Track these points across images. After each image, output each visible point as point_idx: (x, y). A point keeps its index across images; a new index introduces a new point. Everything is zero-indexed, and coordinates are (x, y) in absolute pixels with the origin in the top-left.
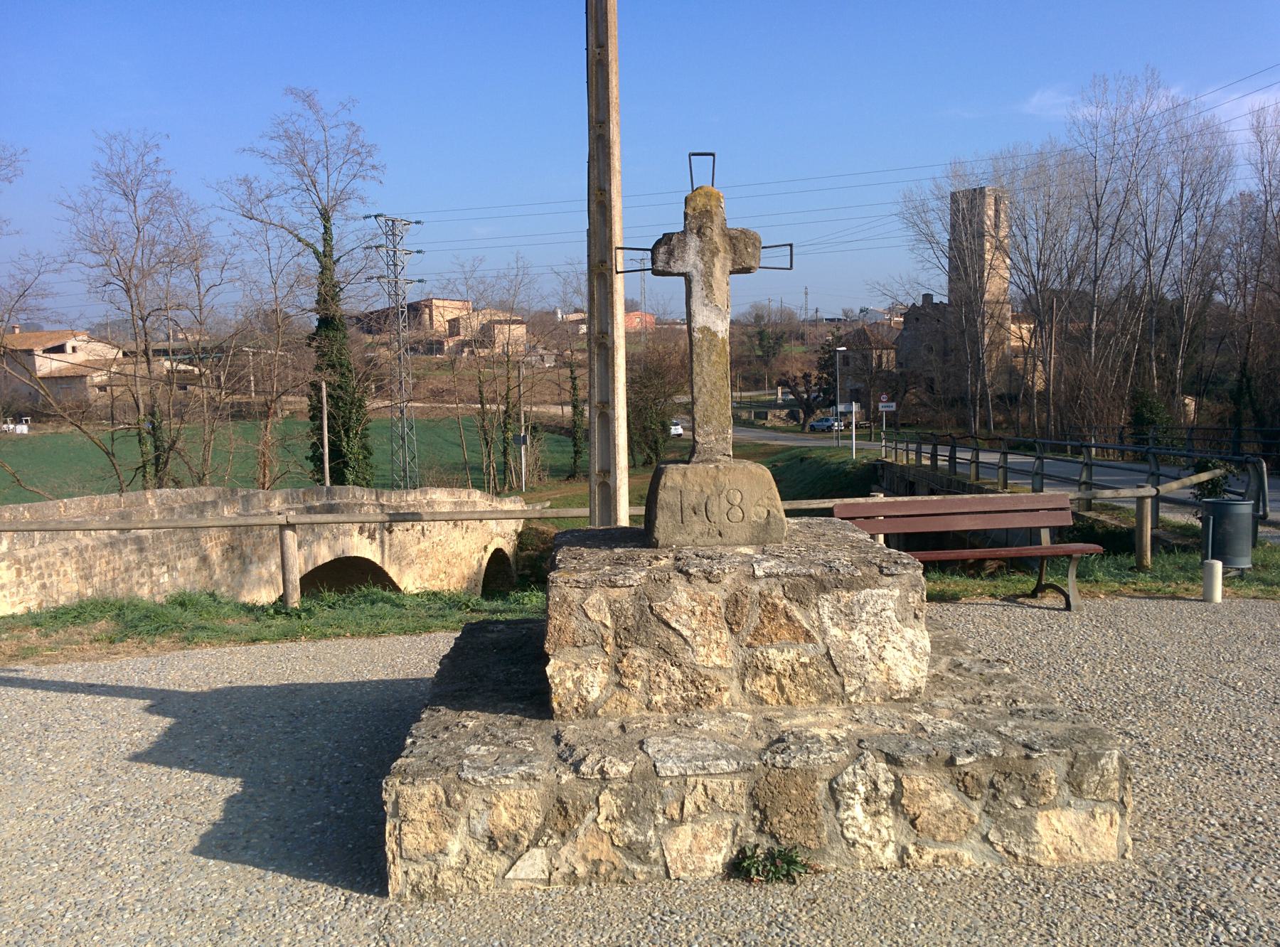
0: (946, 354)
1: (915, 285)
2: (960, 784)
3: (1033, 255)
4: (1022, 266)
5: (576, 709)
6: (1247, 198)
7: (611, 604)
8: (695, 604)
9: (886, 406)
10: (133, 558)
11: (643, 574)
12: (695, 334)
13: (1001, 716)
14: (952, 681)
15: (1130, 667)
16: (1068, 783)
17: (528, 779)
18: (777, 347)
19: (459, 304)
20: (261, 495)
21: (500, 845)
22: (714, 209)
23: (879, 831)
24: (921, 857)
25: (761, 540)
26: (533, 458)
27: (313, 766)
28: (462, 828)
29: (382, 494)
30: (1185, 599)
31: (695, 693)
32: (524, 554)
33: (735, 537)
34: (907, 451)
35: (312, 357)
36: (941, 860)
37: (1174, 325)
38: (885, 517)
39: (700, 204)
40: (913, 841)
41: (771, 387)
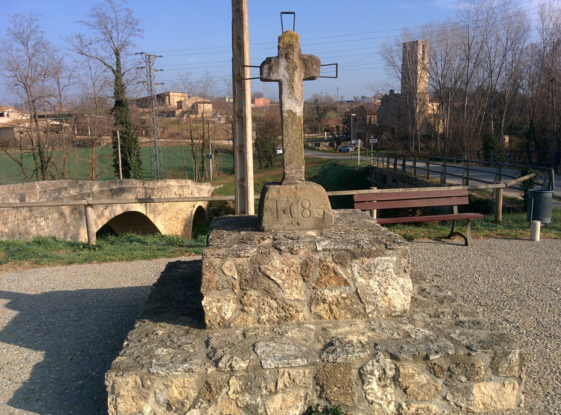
0: (399, 117)
1: (387, 86)
2: (432, 370)
3: (440, 72)
4: (434, 77)
5: (219, 323)
6: (534, 46)
7: (237, 266)
8: (284, 266)
9: (373, 141)
10: (28, 214)
11: (255, 250)
12: (284, 114)
13: (451, 326)
14: (421, 301)
15: (502, 279)
16: (491, 368)
17: (189, 372)
18: (324, 114)
19: (180, 94)
20: (88, 184)
21: (174, 408)
22: (295, 44)
23: (386, 396)
24: (409, 409)
25: (320, 227)
26: (216, 164)
27: (85, 343)
28: (151, 399)
29: (146, 182)
30: (522, 239)
31: (284, 314)
32: (211, 208)
33: (306, 226)
34: (383, 161)
35: (113, 119)
36: (420, 410)
37: (501, 103)
38: (378, 201)
39: (287, 41)
40: (405, 400)
41: (322, 132)
